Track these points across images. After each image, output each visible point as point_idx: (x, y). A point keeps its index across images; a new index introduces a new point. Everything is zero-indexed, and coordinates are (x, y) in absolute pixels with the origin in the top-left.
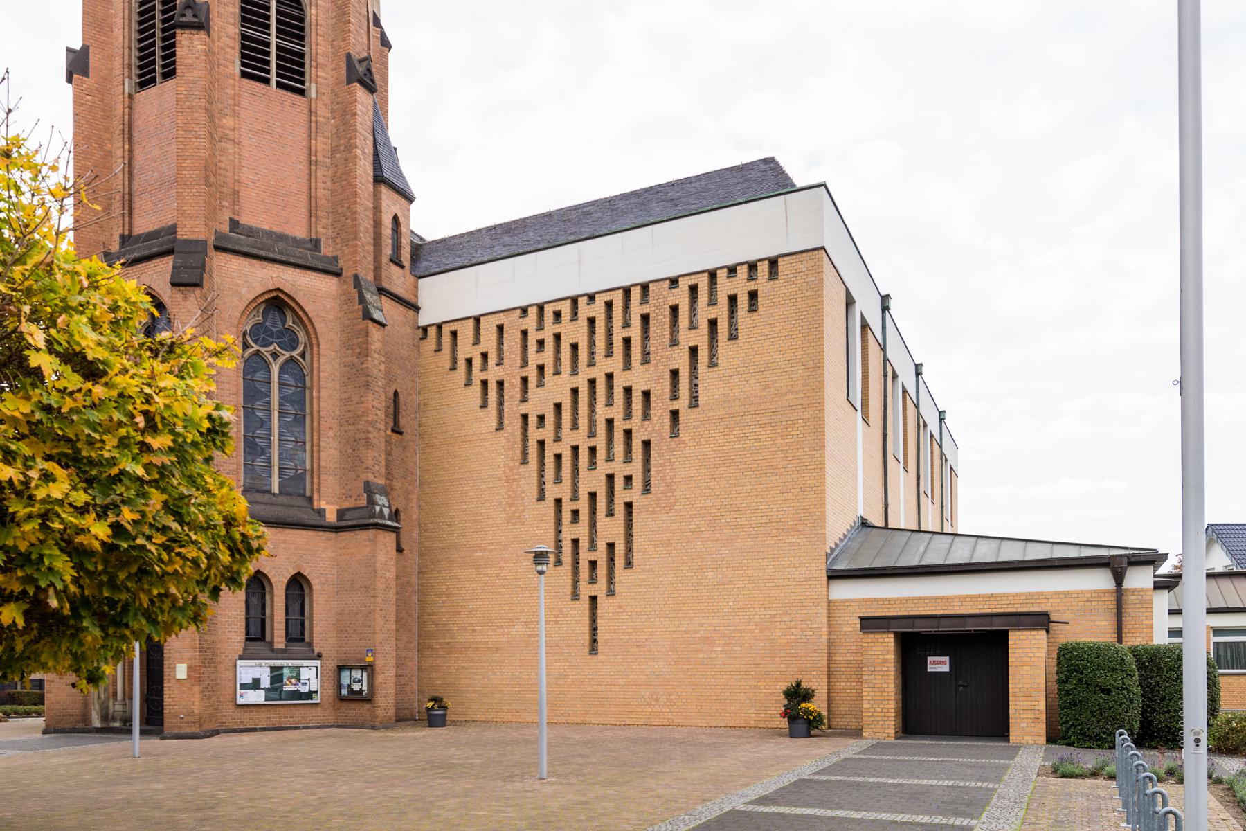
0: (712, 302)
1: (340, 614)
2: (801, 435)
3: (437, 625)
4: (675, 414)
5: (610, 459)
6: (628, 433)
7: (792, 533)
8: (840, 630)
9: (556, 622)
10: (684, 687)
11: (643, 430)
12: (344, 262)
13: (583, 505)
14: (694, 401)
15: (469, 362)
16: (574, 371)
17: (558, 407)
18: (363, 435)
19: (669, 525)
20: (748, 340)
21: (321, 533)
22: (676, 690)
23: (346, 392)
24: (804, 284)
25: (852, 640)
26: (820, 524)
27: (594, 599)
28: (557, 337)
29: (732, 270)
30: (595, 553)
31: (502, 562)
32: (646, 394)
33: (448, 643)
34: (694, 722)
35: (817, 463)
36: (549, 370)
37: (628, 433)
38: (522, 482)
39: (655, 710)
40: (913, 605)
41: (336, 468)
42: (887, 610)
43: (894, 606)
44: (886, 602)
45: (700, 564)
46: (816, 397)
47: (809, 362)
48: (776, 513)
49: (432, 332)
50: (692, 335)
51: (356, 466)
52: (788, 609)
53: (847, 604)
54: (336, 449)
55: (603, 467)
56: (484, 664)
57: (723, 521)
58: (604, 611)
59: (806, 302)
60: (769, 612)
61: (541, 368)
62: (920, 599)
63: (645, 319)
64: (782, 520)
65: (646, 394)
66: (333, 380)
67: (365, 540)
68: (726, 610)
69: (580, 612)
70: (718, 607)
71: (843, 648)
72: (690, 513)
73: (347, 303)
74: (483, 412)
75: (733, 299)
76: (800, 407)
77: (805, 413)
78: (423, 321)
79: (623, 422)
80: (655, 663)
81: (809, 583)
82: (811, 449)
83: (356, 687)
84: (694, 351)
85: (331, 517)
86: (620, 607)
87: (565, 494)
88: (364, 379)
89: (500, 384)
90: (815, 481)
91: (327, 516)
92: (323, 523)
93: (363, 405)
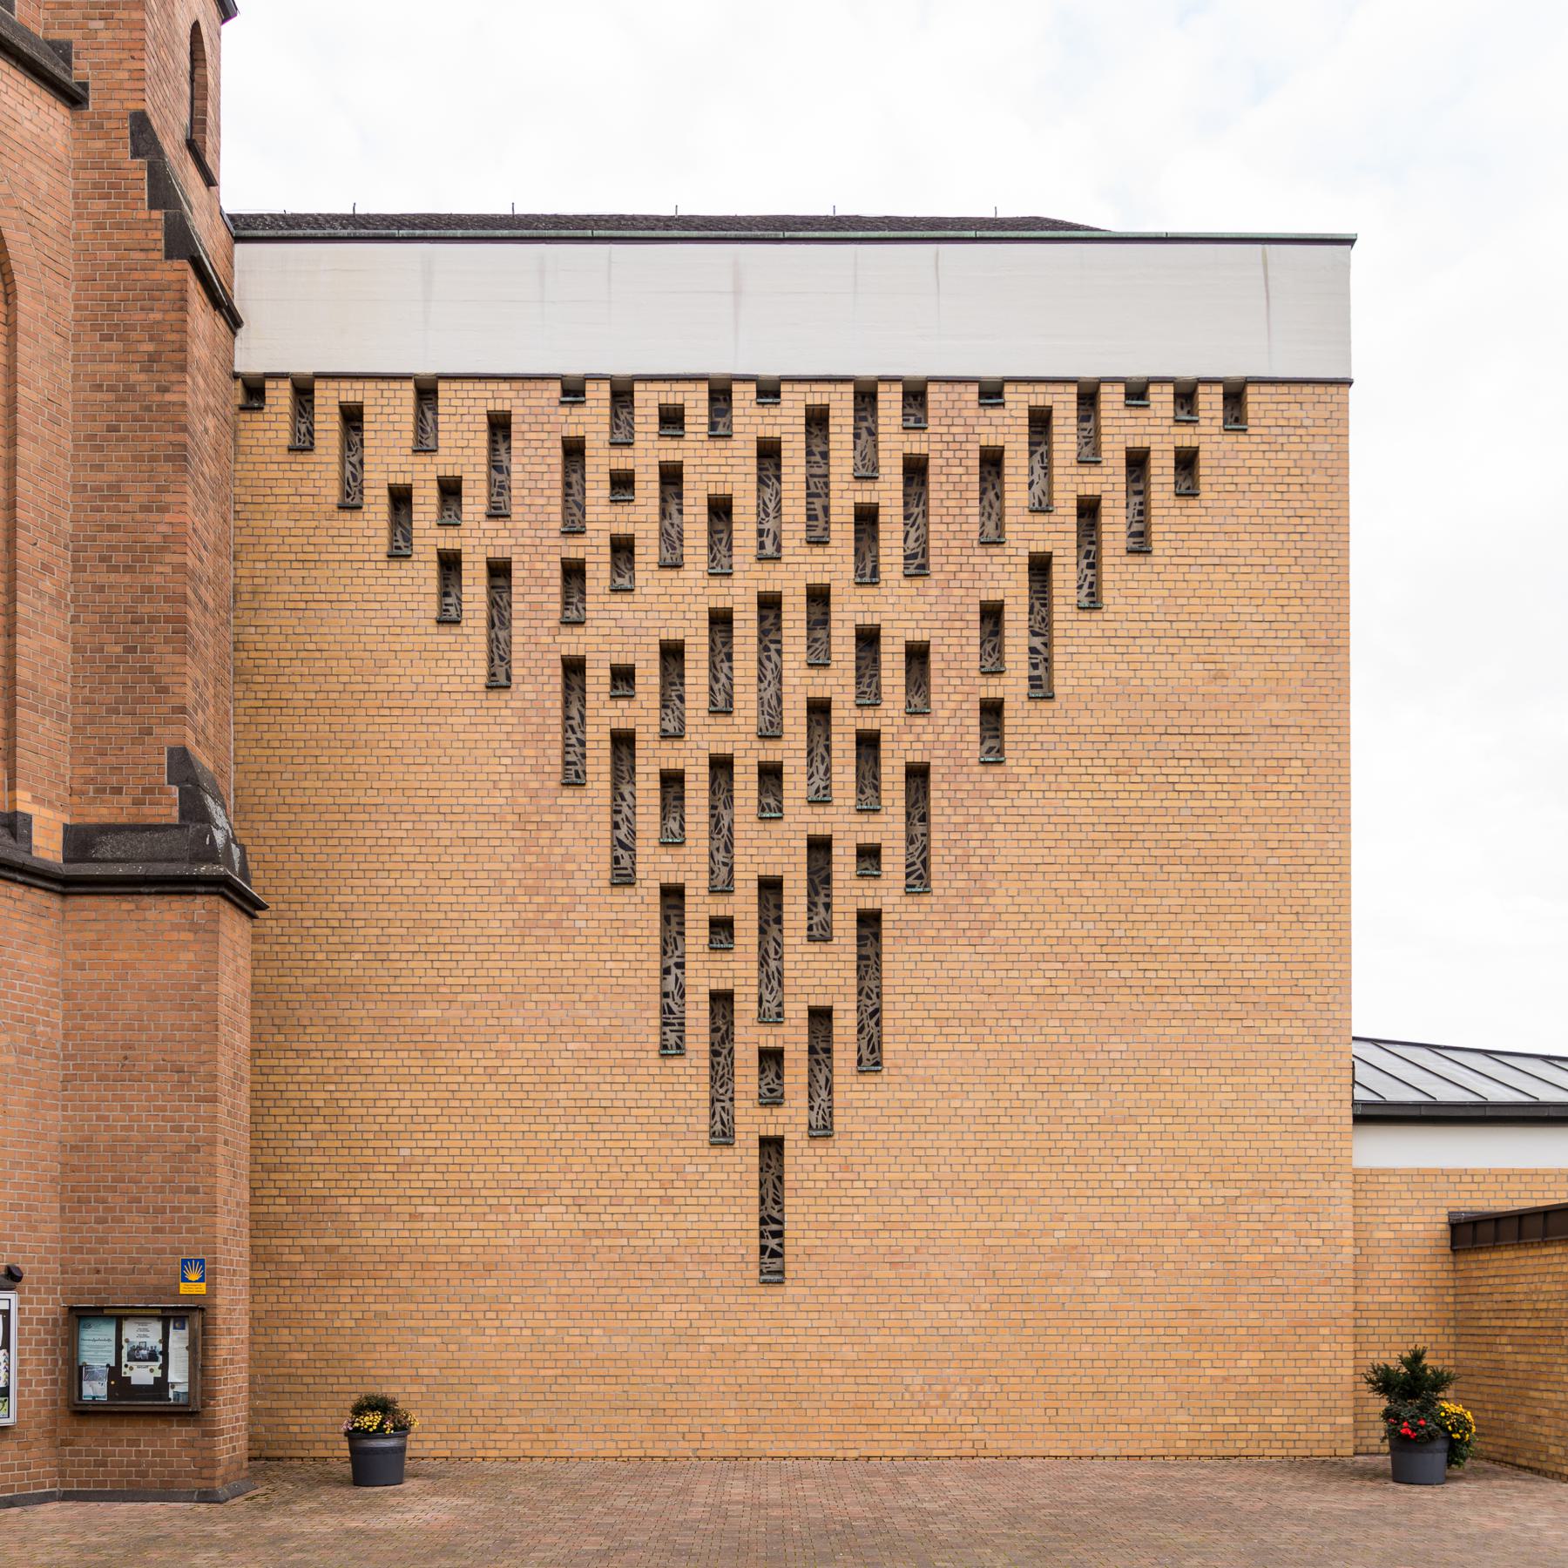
0: (1090, 456)
1: (74, 1148)
2: (1299, 796)
3: (294, 1199)
4: (992, 711)
5: (820, 798)
6: (868, 743)
7: (1276, 1015)
8: (1367, 1235)
9: (667, 1200)
10: (1013, 1364)
11: (911, 737)
12: (94, 66)
13: (744, 907)
14: (1041, 688)
15: (401, 498)
16: (720, 569)
17: (672, 653)
18: (167, 609)
19: (977, 974)
20: (1175, 560)
21: (17, 891)
22: (995, 1372)
23: (99, 468)
24: (1306, 456)
25: (1394, 1259)
26: (1339, 999)
27: (772, 1147)
28: (671, 476)
29: (1137, 393)
30: (777, 1030)
31: (502, 1038)
32: (917, 655)
33: (330, 1249)
34: (1040, 1447)
35: (1333, 861)
36: (648, 552)
37: (868, 743)
38: (567, 832)
39: (937, 1420)
40: (1522, 1187)
41: (61, 697)
42: (1467, 1195)
43: (1482, 1187)
44: (1467, 1179)
45: (1056, 1072)
46: (1331, 714)
47: (1317, 634)
48: (1241, 966)
49: (280, 398)
50: (1039, 527)
51: (141, 701)
52: (1266, 1185)
53: (1382, 1179)
54: (63, 638)
55: (800, 820)
56: (447, 1307)
57: (1114, 974)
58: (802, 1176)
59: (1312, 496)
60: (1222, 1192)
61: (622, 548)
62: (1535, 1173)
63: (915, 470)
64: (1254, 982)
65: (917, 655)
66: (54, 421)
67: (176, 927)
68: (1120, 1184)
69: (736, 1177)
70: (1102, 1176)
71: (1371, 1275)
72: (1031, 949)
73: (107, 197)
74: (447, 637)
75: (1137, 462)
76: (1297, 731)
77: (1306, 746)
78: (252, 357)
79: (857, 713)
80: (940, 1307)
81: (1314, 1128)
82: (1321, 828)
83: (143, 1375)
84: (1040, 567)
85: (47, 846)
86: (846, 1167)
87: (694, 876)
88: (171, 437)
89: (499, 571)
90: (1329, 902)
91: (36, 841)
92: (19, 857)
93: (168, 517)
